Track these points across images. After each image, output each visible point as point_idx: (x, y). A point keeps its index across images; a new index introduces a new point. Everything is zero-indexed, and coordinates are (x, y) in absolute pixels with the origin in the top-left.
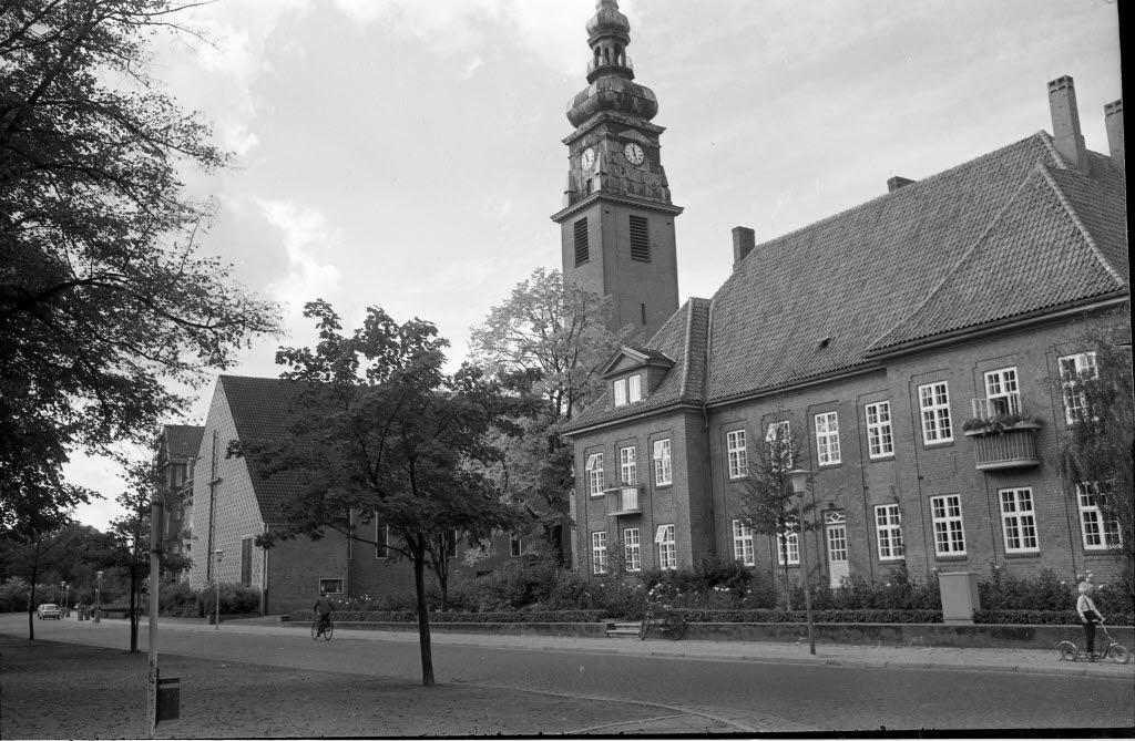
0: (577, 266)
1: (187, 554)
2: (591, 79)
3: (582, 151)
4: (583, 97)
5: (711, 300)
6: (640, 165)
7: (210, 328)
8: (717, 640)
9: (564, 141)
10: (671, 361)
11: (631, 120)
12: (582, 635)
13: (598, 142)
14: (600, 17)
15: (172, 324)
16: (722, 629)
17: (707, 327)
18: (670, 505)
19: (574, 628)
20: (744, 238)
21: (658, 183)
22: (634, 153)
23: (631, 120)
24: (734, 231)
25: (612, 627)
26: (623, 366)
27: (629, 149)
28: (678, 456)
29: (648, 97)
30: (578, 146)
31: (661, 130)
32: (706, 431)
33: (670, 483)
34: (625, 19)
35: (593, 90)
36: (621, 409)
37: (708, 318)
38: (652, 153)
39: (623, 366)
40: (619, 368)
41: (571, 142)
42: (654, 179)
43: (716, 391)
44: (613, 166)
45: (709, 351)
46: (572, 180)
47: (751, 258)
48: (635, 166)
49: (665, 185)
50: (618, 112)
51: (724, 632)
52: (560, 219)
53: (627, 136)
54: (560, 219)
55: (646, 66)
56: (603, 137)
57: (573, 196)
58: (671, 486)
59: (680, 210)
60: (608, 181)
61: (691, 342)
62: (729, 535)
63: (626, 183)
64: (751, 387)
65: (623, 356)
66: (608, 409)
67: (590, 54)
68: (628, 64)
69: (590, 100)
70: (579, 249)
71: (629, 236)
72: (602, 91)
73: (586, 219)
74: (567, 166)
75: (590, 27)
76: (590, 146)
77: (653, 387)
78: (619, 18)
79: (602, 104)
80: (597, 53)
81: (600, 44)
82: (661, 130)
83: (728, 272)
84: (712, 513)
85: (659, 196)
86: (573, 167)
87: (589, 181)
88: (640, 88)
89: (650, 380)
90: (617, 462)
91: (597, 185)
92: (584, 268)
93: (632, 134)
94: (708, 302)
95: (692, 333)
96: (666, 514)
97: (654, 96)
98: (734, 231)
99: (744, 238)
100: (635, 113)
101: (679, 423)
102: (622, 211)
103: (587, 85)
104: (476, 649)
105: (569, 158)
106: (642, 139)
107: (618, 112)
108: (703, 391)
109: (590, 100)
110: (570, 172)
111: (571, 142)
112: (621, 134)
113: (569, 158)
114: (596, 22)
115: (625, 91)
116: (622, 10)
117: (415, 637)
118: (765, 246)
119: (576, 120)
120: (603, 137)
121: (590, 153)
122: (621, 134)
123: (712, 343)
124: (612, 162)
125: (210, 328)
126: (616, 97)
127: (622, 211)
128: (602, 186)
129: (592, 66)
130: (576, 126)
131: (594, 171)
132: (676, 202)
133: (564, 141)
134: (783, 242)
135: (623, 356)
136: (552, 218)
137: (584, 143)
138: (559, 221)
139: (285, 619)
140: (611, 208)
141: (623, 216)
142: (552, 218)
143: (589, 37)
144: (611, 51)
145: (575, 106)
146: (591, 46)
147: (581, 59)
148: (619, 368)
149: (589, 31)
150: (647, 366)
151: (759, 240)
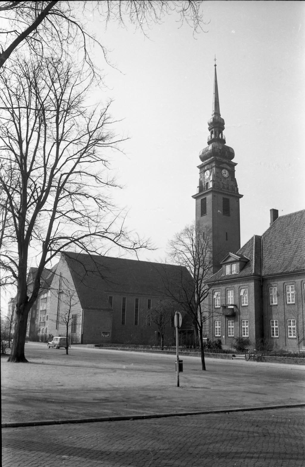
0: (201, 216)
1: (217, 341)
2: (209, 143)
3: (205, 171)
4: (206, 150)
5: (262, 236)
6: (227, 178)
7: (134, 249)
8: (276, 363)
9: (198, 167)
10: (247, 259)
11: (225, 160)
12: (222, 358)
13: (212, 168)
14: (214, 119)
15: (184, 264)
16: (277, 359)
17: (261, 247)
18: (247, 313)
19: (219, 355)
20: (275, 213)
21: (234, 185)
22: (225, 173)
23: (225, 160)
24: (271, 210)
25: (234, 356)
26: (230, 260)
27: (223, 171)
28: (251, 295)
29: (231, 151)
30: (203, 169)
31: (236, 164)
32: (261, 287)
33: (247, 305)
34: (223, 120)
35: (210, 147)
36: (228, 276)
37: (261, 243)
38: (232, 173)
39: (230, 260)
40: (228, 261)
41: (201, 167)
42: (232, 183)
43: (264, 272)
44: (217, 178)
45: (262, 256)
46: (201, 182)
47: (278, 222)
48: (225, 178)
49: (237, 186)
50: (220, 158)
51: (278, 360)
52: (196, 197)
53: (223, 167)
54: (196, 197)
55: (230, 137)
56: (213, 167)
57: (201, 188)
58: (248, 306)
59: (242, 196)
60: (215, 184)
61: (256, 253)
62: (269, 325)
63: (222, 185)
64: (280, 271)
65: (230, 256)
66: (223, 275)
67: (209, 133)
68: (223, 138)
69: (209, 151)
70: (202, 210)
71: (222, 205)
72: (214, 148)
73: (206, 198)
74: (198, 177)
75: (209, 122)
76: (208, 169)
77: (242, 268)
78: (221, 120)
79: (214, 153)
80: (212, 133)
81: (213, 130)
82: (236, 164)
83: (268, 226)
84: (263, 317)
85: (234, 190)
86: (201, 177)
87: (207, 183)
88: (228, 148)
89: (240, 265)
90: (226, 295)
91: (211, 185)
92: (204, 217)
93: (225, 165)
94: (261, 237)
95: (255, 249)
96: (245, 316)
97: (233, 151)
98: (271, 210)
99: (275, 213)
100: (225, 157)
101: (252, 284)
102: (220, 197)
103: (207, 145)
104: (132, 354)
105: (200, 173)
106: (228, 167)
107: (220, 158)
108: (261, 272)
109: (209, 151)
110: (200, 179)
111: (201, 167)
112: (221, 166)
113: (200, 173)
114: (212, 120)
115: (222, 149)
116: (222, 117)
117: (200, 359)
118: (283, 217)
119: (203, 158)
120: (213, 167)
121: (208, 172)
122: (221, 166)
123: (263, 253)
124: (217, 176)
125: (134, 249)
126: (219, 151)
127: (220, 197)
128: (213, 186)
129: (210, 138)
130: (203, 161)
131: (210, 179)
132: (240, 192)
133: (198, 167)
134: (290, 216)
135: (230, 256)
136: (192, 196)
137: (206, 168)
138: (195, 198)
139: (96, 346)
140: (216, 195)
141: (220, 197)
142: (192, 196)
143: (208, 127)
144: (217, 132)
145: (203, 153)
146: (210, 130)
147: (207, 135)
148: (228, 261)
149: (209, 124)
150: (240, 261)
151: (280, 214)
